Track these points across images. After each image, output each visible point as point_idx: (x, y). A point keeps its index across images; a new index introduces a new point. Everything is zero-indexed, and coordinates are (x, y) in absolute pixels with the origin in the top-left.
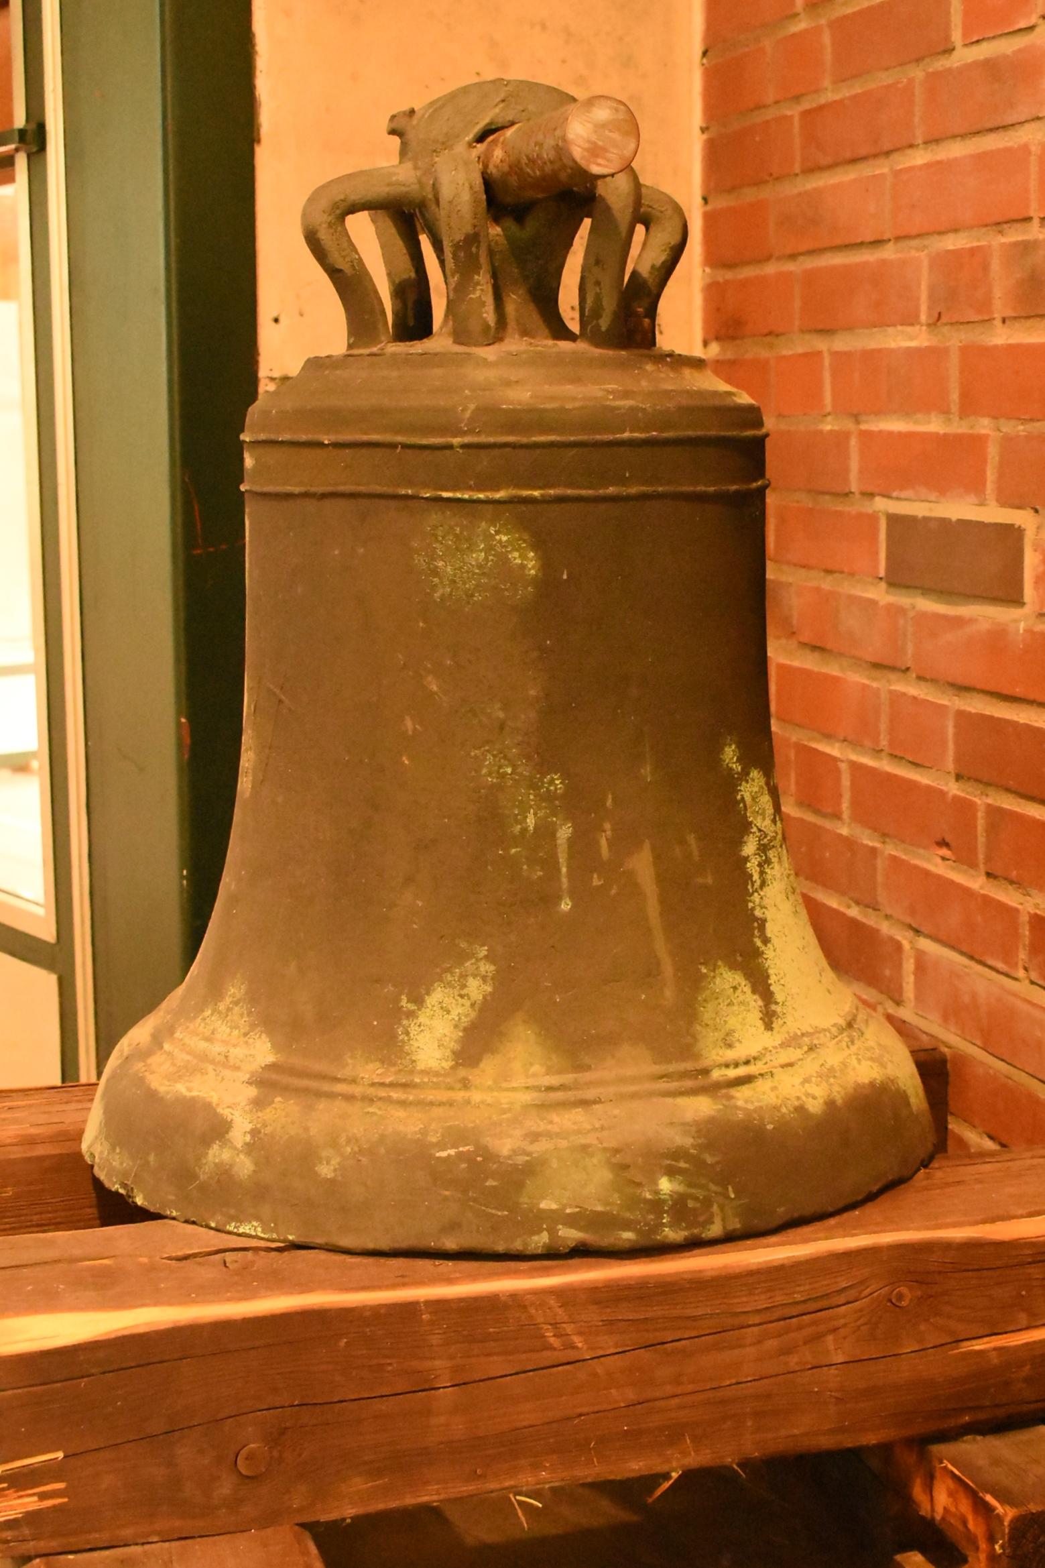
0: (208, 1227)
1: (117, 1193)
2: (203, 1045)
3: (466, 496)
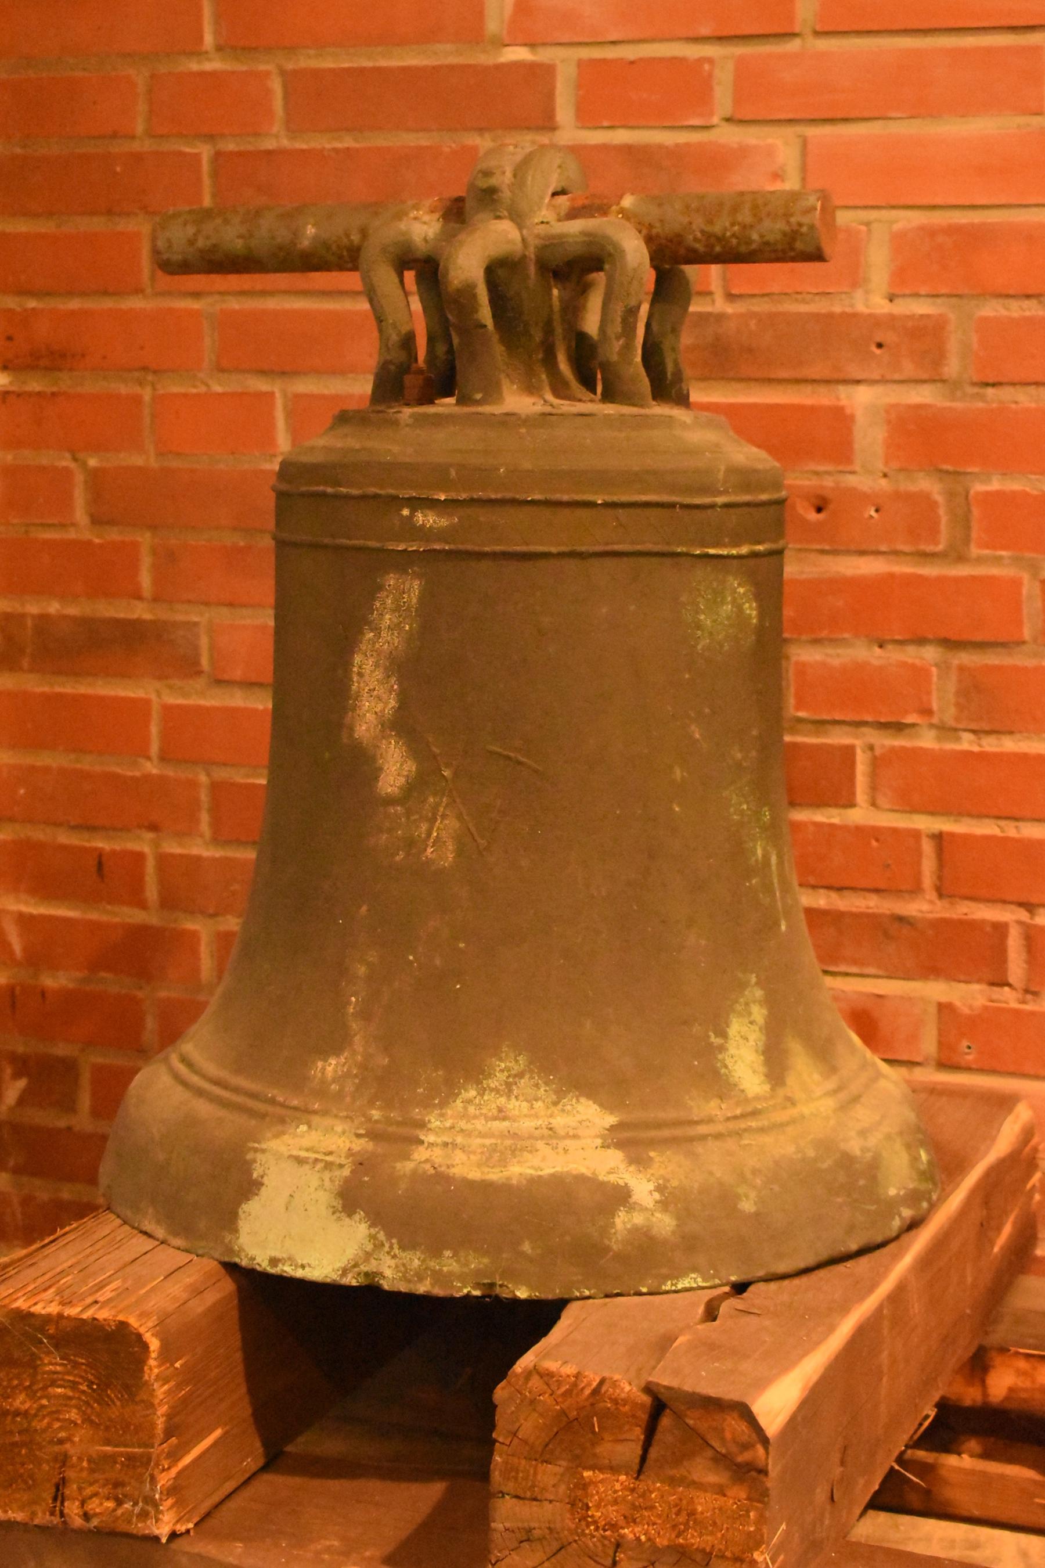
0: (641, 1294)
1: (468, 1296)
2: (497, 1125)
3: (725, 553)
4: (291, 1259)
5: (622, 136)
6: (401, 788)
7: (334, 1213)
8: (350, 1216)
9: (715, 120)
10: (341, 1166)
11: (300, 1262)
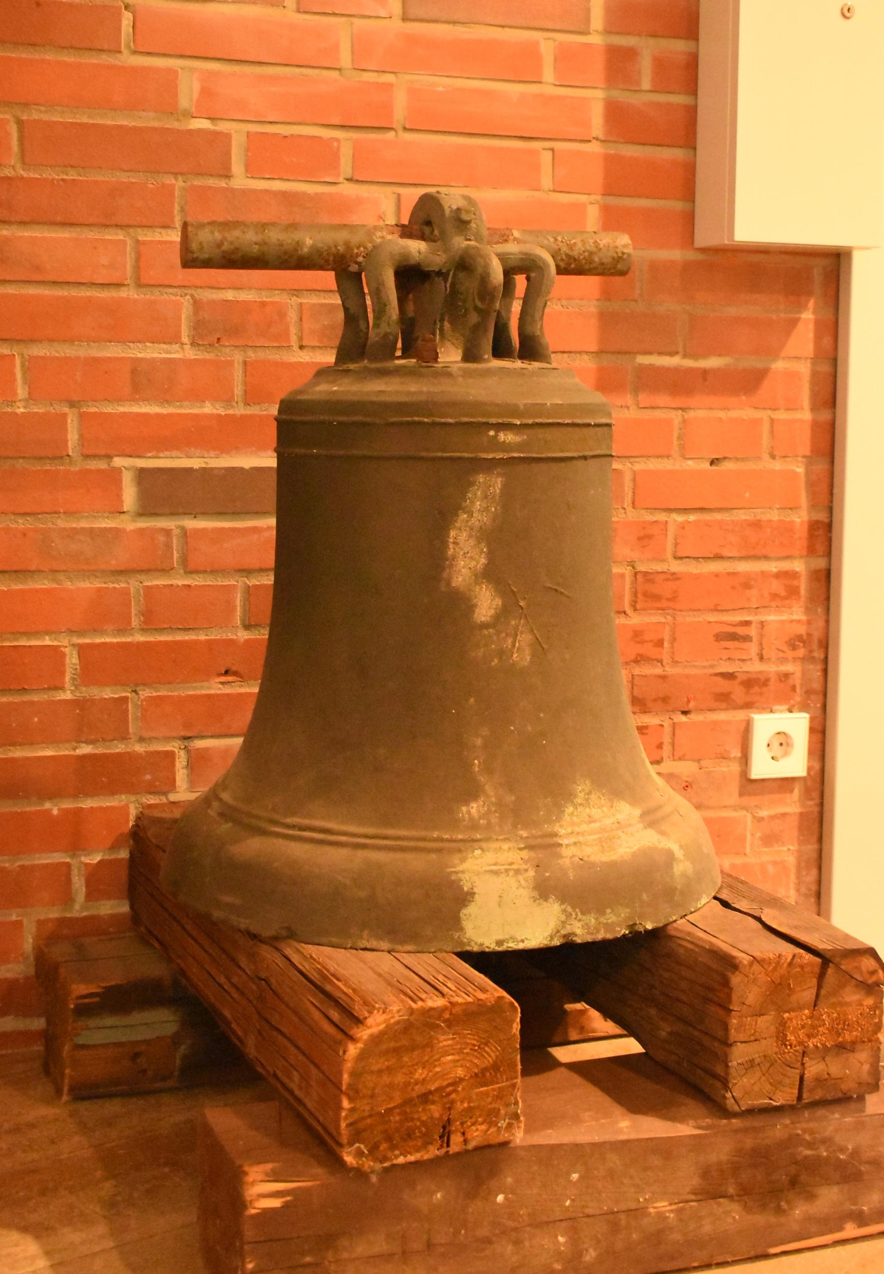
2: (593, 825)
4: (513, 939)
5: (277, 186)
6: (491, 617)
7: (535, 901)
8: (546, 900)
9: (341, 180)
10: (526, 870)
11: (520, 939)
